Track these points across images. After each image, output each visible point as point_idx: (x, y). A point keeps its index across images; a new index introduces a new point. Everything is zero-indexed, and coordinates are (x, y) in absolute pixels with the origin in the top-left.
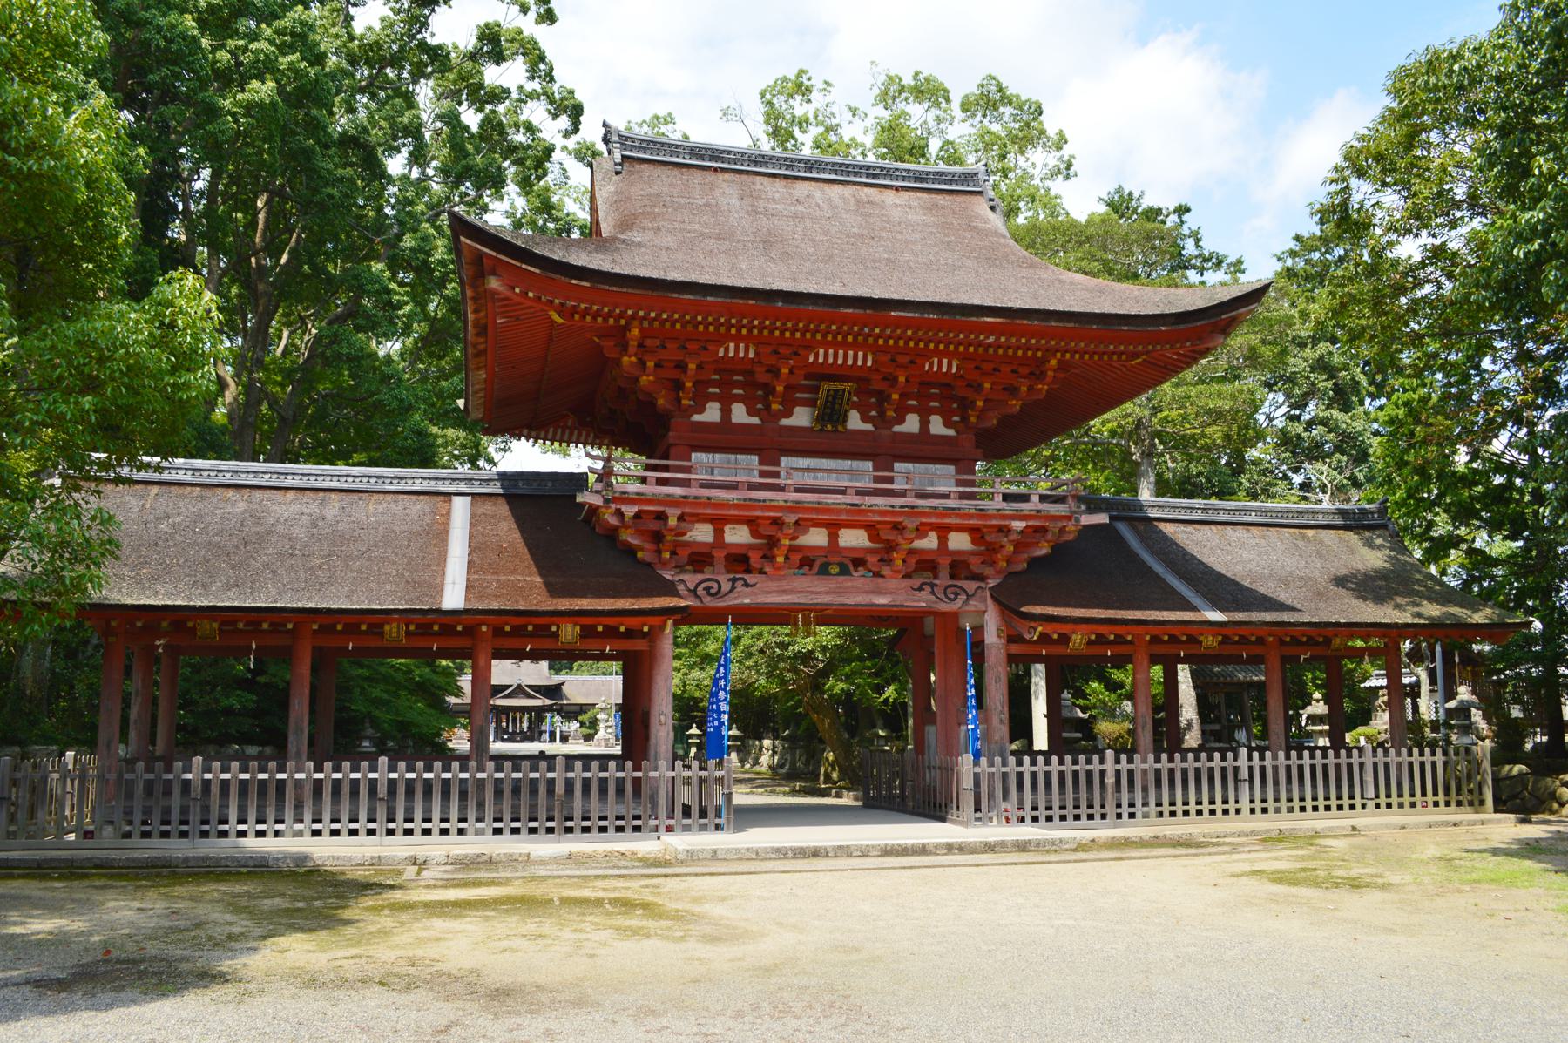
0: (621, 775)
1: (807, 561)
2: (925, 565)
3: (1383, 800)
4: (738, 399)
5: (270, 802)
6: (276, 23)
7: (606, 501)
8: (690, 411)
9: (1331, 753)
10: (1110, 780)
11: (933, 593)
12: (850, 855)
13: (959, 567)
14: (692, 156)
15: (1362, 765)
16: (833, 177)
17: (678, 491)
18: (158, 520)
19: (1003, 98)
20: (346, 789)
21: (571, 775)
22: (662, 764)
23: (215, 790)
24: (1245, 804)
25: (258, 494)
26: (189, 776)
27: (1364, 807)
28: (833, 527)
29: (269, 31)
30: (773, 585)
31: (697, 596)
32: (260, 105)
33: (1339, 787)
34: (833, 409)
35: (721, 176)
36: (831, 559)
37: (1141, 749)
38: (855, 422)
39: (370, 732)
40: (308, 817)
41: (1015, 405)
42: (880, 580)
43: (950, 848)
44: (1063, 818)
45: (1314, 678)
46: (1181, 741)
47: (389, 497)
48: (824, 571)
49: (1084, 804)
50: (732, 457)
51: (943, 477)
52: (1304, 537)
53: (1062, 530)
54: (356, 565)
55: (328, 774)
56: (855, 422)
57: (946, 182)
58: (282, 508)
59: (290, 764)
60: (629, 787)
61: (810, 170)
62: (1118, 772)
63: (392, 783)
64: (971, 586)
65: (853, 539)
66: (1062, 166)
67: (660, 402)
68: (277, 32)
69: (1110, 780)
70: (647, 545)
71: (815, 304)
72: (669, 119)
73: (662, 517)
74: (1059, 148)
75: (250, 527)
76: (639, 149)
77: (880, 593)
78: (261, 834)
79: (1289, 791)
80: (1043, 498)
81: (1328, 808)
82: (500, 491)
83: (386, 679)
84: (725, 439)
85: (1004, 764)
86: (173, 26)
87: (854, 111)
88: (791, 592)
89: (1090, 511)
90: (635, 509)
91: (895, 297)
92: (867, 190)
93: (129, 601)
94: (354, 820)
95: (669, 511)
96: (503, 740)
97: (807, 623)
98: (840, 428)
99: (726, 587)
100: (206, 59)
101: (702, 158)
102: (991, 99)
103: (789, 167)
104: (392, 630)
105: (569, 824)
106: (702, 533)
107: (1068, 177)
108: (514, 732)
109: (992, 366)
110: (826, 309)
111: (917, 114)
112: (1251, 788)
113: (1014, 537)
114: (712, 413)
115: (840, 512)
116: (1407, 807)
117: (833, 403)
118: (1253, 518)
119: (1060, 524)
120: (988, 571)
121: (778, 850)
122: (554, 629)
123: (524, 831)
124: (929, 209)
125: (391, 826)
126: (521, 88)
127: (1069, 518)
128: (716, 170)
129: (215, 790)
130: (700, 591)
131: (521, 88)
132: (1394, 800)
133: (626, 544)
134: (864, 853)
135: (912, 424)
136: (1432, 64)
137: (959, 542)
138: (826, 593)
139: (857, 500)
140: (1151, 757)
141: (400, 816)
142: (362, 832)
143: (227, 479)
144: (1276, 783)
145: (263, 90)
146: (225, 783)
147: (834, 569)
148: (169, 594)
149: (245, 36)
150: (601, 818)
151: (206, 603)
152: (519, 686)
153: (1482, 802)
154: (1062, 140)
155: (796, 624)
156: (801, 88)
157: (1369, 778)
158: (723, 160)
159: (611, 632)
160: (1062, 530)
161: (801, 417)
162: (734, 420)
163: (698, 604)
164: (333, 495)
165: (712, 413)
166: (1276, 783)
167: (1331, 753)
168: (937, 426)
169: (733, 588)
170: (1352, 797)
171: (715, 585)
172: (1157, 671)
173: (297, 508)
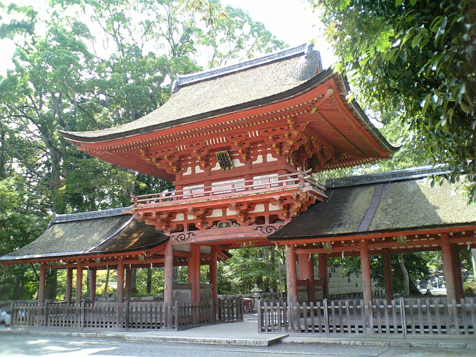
2: (260, 220)
11: (261, 230)
38: (237, 163)
39: (270, 287)
56: (237, 163)
84: (194, 180)
90: (279, 196)
122: (394, 238)
130: (179, 239)
135: (260, 159)
136: (84, 45)
138: (221, 235)
142: (467, 333)
147: (224, 225)
162: (268, 161)
165: (189, 172)
169: (189, 237)
172: (205, 269)
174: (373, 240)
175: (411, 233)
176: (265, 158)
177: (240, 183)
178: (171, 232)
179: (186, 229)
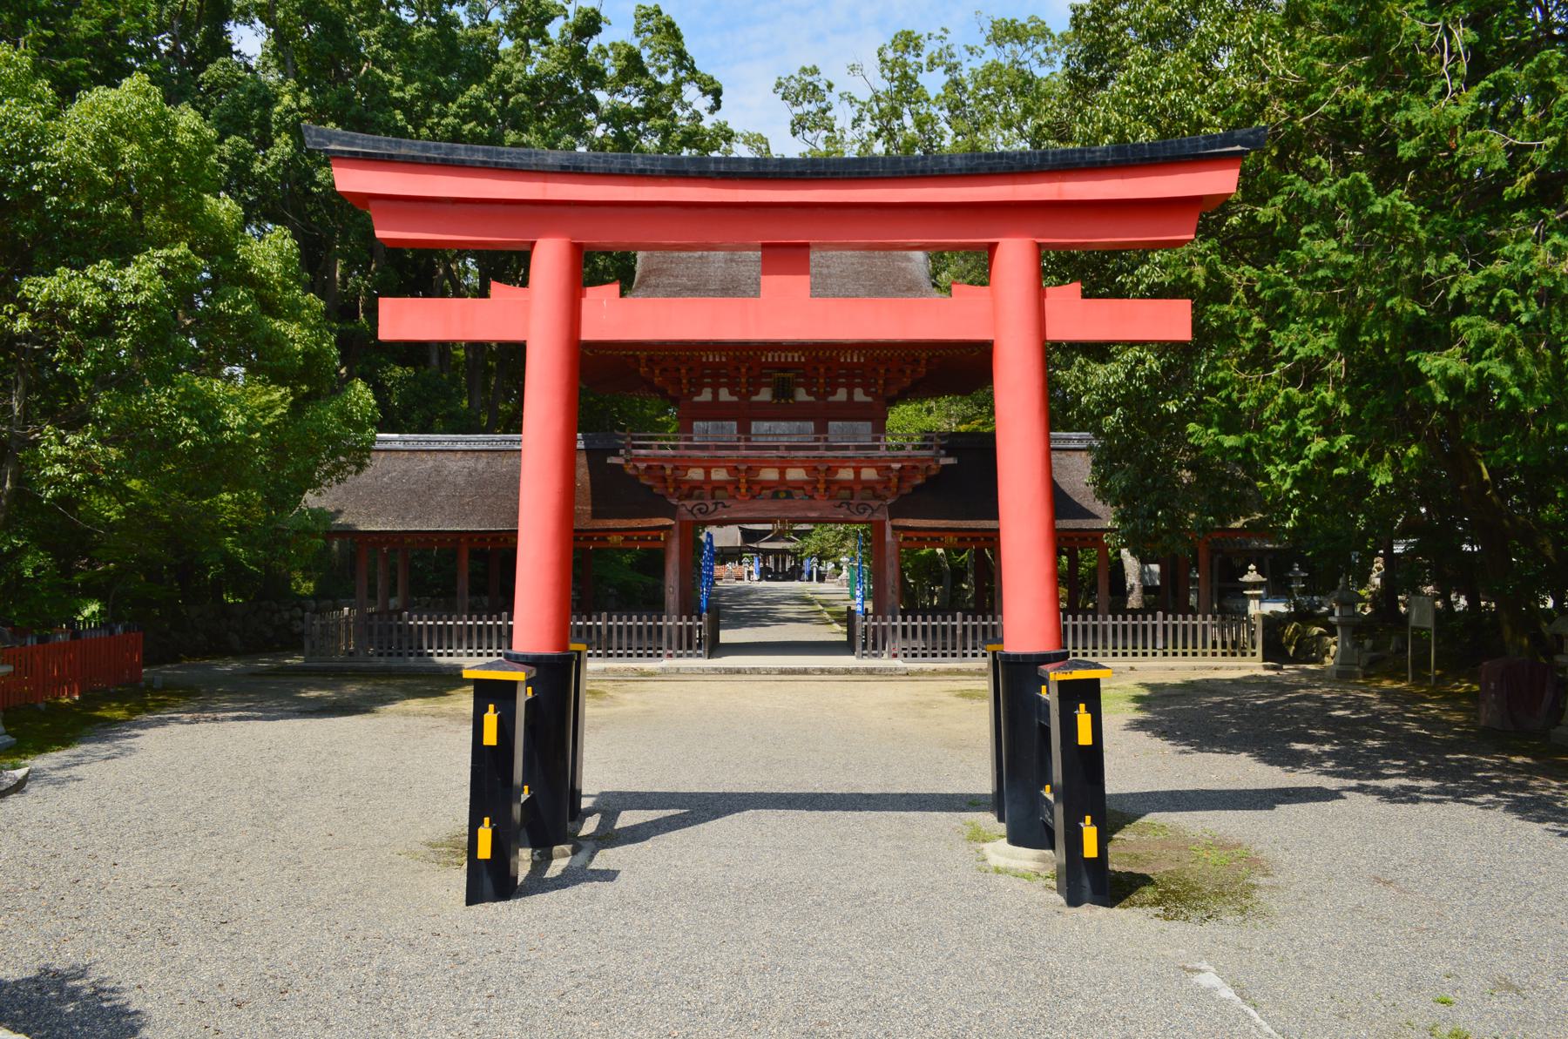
5: (445, 637)
10: (959, 632)
15: (1154, 627)
17: (671, 452)
25: (440, 455)
38: (801, 395)
43: (822, 671)
46: (1126, 602)
48: (775, 496)
49: (949, 646)
53: (928, 468)
56: (801, 395)
64: (875, 504)
65: (796, 474)
68: (460, 107)
69: (959, 632)
72: (815, 71)
73: (663, 468)
80: (914, 447)
84: (715, 412)
87: (971, 51)
89: (947, 456)
106: (696, 474)
114: (706, 396)
120: (887, 493)
134: (768, 672)
135: (841, 395)
137: (869, 474)
139: (785, 454)
143: (424, 446)
147: (783, 495)
148: (384, 524)
157: (1160, 635)
160: (928, 468)
161: (765, 395)
168: (859, 396)
173: (461, 464)
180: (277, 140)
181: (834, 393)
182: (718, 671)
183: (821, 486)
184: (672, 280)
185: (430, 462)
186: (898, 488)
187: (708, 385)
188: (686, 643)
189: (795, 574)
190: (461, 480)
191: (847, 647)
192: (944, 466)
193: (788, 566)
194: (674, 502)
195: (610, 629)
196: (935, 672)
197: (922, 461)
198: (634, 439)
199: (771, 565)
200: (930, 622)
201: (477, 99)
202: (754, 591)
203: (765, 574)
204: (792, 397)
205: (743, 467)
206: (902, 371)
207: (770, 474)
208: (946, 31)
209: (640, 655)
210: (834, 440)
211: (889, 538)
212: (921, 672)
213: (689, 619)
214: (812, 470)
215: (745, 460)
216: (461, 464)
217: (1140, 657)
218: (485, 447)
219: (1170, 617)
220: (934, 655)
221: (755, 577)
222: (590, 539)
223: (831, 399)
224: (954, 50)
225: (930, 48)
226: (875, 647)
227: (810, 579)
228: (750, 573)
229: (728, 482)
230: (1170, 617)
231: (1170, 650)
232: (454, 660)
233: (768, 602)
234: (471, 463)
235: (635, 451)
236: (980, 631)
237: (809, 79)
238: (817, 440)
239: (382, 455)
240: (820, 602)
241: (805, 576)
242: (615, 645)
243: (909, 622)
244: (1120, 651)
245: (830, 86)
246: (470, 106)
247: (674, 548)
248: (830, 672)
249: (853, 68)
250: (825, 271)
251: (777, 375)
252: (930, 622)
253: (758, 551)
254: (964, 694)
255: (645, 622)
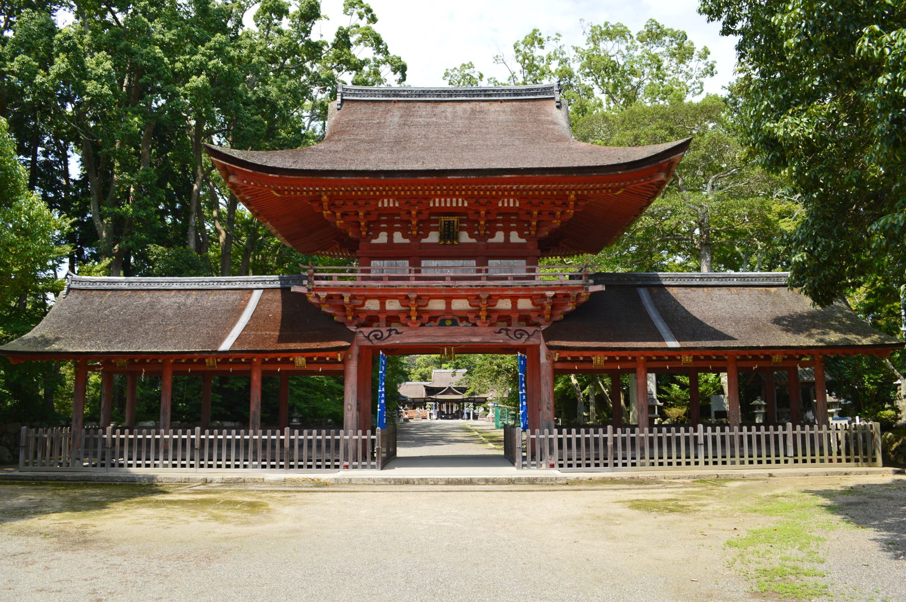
0: (364, 437)
1: (435, 319)
2: (505, 318)
3: (800, 457)
4: (397, 229)
5: (145, 450)
6: (207, 44)
7: (309, 290)
8: (368, 238)
9: (763, 428)
10: (610, 443)
11: (507, 334)
12: (427, 484)
13: (525, 318)
14: (383, 95)
15: (785, 436)
16: (464, 98)
18: (106, 308)
19: (662, 32)
20: (180, 444)
21: (292, 437)
22: (350, 431)
23: (118, 443)
24: (701, 459)
25: (157, 294)
26: (105, 436)
27: (786, 462)
28: (382, 299)
29: (203, 49)
30: (413, 332)
31: (371, 341)
32: (197, 88)
33: (777, 449)
34: (449, 231)
35: (397, 105)
36: (447, 317)
37: (640, 425)
39: (296, 414)
40: (170, 457)
41: (557, 223)
42: (476, 328)
43: (487, 481)
44: (579, 465)
45: (870, 378)
47: (221, 292)
48: (443, 324)
49: (601, 457)
50: (394, 262)
51: (519, 267)
52: (767, 292)
53: (579, 295)
54: (187, 329)
55: (180, 436)
56: (464, 238)
57: (533, 94)
58: (167, 300)
59: (251, 431)
60: (324, 444)
61: (451, 96)
62: (615, 439)
63: (202, 440)
64: (531, 330)
65: (460, 305)
66: (709, 68)
67: (350, 234)
69: (610, 443)
70: (337, 313)
71: (402, 176)
72: (471, 66)
73: (342, 298)
74: (706, 58)
75: (148, 310)
76: (354, 95)
77: (475, 335)
78: (139, 466)
79: (741, 451)
81: (760, 462)
82: (279, 286)
83: (308, 385)
84: (390, 252)
85: (550, 433)
86: (149, 53)
88: (423, 336)
89: (595, 284)
90: (326, 294)
91: (449, 168)
92: (482, 104)
93: (71, 350)
94: (184, 460)
95: (344, 294)
96: (442, 418)
97: (449, 352)
98: (455, 242)
99: (386, 334)
100: (167, 68)
101: (389, 96)
102: (654, 34)
103: (438, 96)
104: (777, 358)
105: (292, 463)
106: (373, 305)
107: (712, 75)
108: (448, 414)
109: (538, 201)
110: (410, 178)
111: (609, 47)
112: (706, 449)
113: (548, 300)
114: (383, 238)
115: (441, 290)
116: (773, 464)
117: (449, 229)
118: (735, 282)
119: (577, 292)
120: (541, 321)
121: (386, 480)
123: (268, 467)
124: (514, 112)
125: (202, 463)
126: (375, 59)
127: (582, 288)
128: (395, 102)
129: (118, 443)
130: (371, 337)
131: (375, 59)
132: (817, 457)
133: (326, 314)
134: (436, 482)
135: (499, 237)
137: (524, 304)
139: (451, 283)
140: (646, 429)
141: (206, 458)
142: (188, 466)
143: (145, 286)
144: (732, 446)
145: (197, 81)
146: (122, 440)
147: (449, 323)
149: (189, 53)
150: (318, 461)
151: (106, 350)
152: (450, 388)
153: (874, 460)
154: (707, 52)
155: (443, 353)
156: (535, 39)
157: (790, 443)
158: (400, 96)
159: (321, 361)
160: (579, 295)
163: (370, 344)
164: (194, 292)
165: (383, 238)
166: (732, 446)
167: (763, 428)
168: (515, 238)
169: (390, 335)
170: (777, 455)
171: (380, 334)
173: (173, 300)
174: (618, 358)
175: (696, 353)
176: (390, 237)
177: (469, 266)
178: (358, 326)
179: (383, 322)
180: (56, 59)
181: (493, 236)
182: (388, 481)
183: (483, 315)
184: (352, 137)
185: (147, 298)
186: (551, 315)
187: (384, 230)
188: (364, 455)
189: (458, 415)
190: (170, 313)
191: (509, 458)
192: (594, 293)
193: (454, 410)
194: (353, 329)
195: (292, 441)
196: (591, 481)
197: (573, 289)
198: (315, 271)
199: (445, 410)
200: (583, 435)
201: (221, 43)
202: (435, 425)
203: (441, 415)
204: (457, 238)
205: (413, 295)
206: (552, 214)
207: (438, 305)
208: (559, 36)
209: (319, 467)
210: (493, 273)
211: (543, 359)
212: (578, 482)
213: (364, 434)
214: (474, 298)
215: (414, 289)
216: (173, 300)
217: (666, 466)
218: (196, 287)
219: (798, 427)
220: (588, 465)
221: (434, 417)
222: (273, 361)
223: (490, 240)
224: (564, 49)
225: (550, 48)
226: (533, 457)
227: (469, 418)
228: (431, 414)
229: (400, 312)
230: (798, 427)
231: (800, 457)
232: (151, 471)
233: (442, 430)
234: (182, 300)
235: (317, 282)
236: (628, 442)
237: (467, 71)
238: (479, 271)
239: (109, 293)
240: (476, 430)
241: (465, 416)
242: (296, 457)
243: (565, 435)
244: (764, 459)
245: (481, 76)
246: (216, 49)
247: (352, 368)
248: (494, 482)
249: (496, 59)
250: (484, 130)
251: (443, 219)
252: (591, 435)
253: (436, 401)
254: (637, 505)
255: (324, 436)
